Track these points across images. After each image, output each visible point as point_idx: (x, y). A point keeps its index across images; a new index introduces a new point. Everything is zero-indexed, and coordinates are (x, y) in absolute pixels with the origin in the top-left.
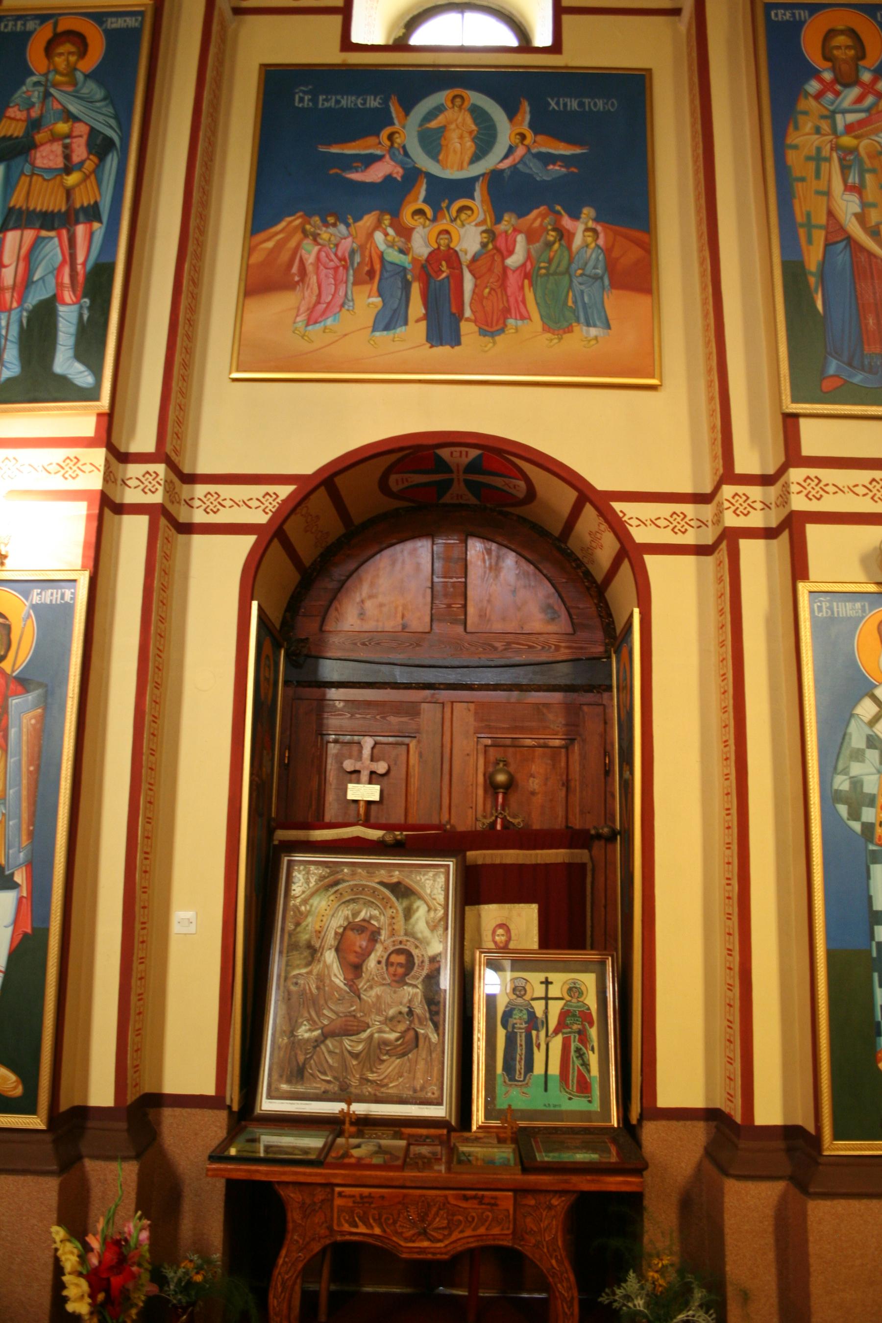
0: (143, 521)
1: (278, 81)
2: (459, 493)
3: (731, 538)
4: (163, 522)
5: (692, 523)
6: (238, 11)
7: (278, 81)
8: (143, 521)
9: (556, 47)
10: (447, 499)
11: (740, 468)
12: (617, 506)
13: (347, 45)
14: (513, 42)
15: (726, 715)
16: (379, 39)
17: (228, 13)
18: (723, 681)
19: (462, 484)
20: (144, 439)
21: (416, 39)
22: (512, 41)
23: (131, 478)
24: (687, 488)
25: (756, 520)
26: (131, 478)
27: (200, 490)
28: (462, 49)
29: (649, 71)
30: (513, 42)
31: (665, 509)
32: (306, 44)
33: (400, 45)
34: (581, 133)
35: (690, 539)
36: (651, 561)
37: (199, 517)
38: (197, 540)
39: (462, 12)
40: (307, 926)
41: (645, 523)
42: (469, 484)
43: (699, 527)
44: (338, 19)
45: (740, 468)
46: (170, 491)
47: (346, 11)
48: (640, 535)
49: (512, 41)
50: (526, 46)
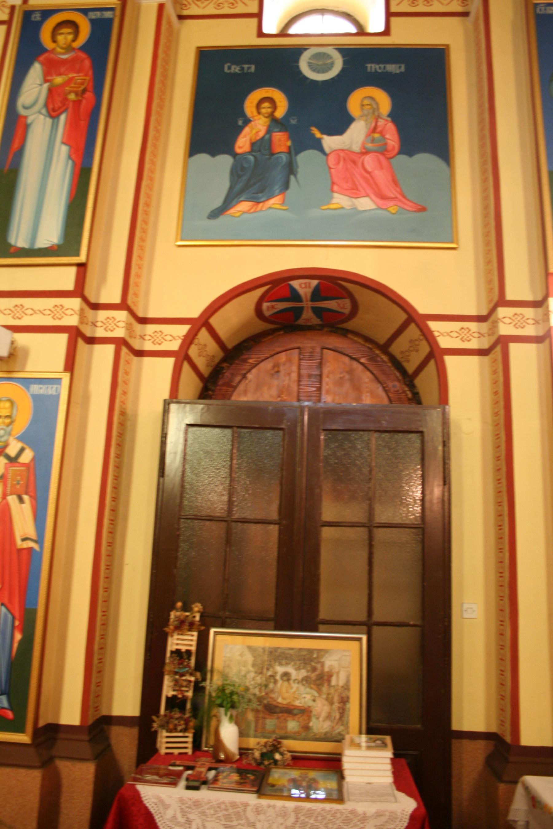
0: (110, 349)
1: (208, 58)
2: (308, 316)
3: (503, 342)
4: (124, 350)
5: (474, 335)
6: (181, 17)
7: (208, 58)
8: (110, 349)
9: (387, 32)
10: (300, 322)
11: (510, 296)
12: (433, 325)
13: (261, 34)
14: (354, 30)
15: (499, 462)
16: (274, 31)
17: (174, 19)
18: (498, 439)
19: (310, 311)
20: (111, 293)
21: (291, 31)
22: (353, 29)
23: (123, 327)
24: (473, 312)
25: (530, 331)
26: (123, 327)
27: (150, 328)
28: (322, 35)
29: (448, 46)
30: (354, 30)
31: (456, 326)
32: (235, 35)
33: (283, 34)
34: (413, 84)
35: (473, 345)
36: (449, 360)
37: (148, 346)
38: (147, 360)
39: (323, 15)
40: (21, 500)
41: (446, 335)
42: (317, 311)
43: (479, 337)
44: (255, 21)
45: (510, 296)
46: (129, 328)
47: (259, 16)
48: (444, 343)
49: (353, 29)
50: (362, 32)
